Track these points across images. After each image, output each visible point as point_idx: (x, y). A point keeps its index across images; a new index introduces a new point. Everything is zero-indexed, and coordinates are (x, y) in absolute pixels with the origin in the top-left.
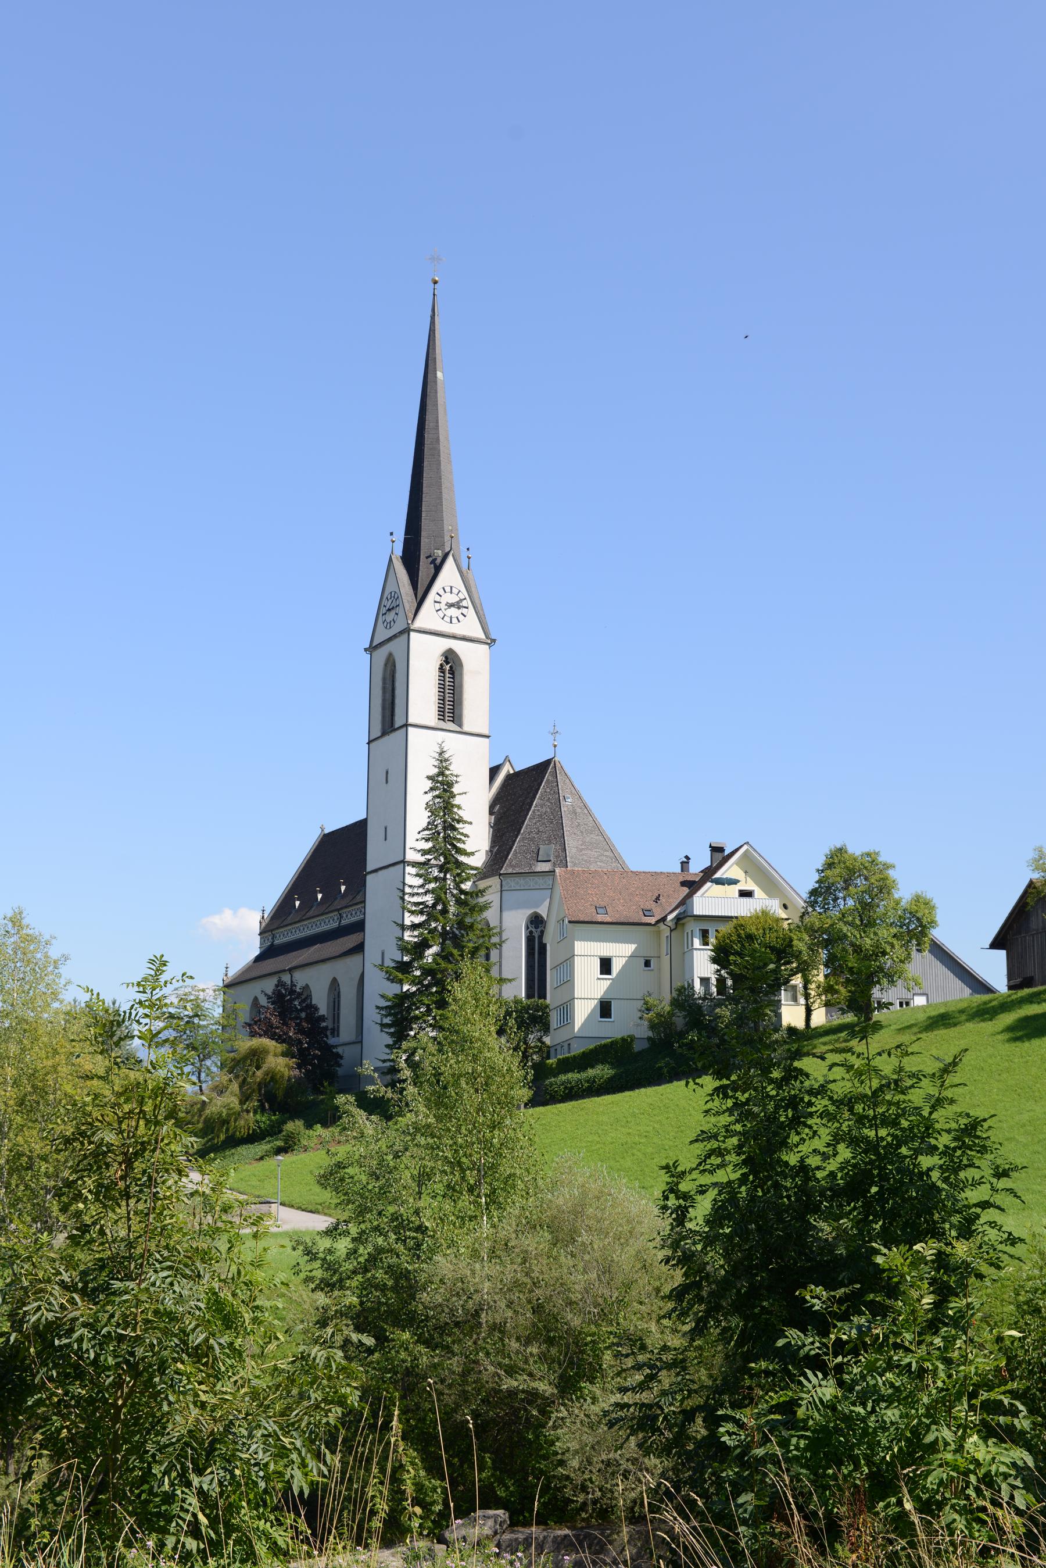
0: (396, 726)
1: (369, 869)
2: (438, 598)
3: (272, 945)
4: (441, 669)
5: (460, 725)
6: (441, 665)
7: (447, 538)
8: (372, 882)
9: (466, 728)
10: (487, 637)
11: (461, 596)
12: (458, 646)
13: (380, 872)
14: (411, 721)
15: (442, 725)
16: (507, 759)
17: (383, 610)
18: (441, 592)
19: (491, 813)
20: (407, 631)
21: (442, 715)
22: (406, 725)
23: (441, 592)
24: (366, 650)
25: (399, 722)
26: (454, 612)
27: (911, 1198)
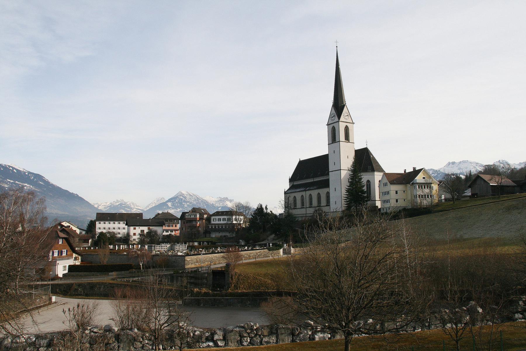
5: (349, 141)
9: (350, 142)
12: (348, 124)
13: (333, 172)
20: (339, 122)
25: (337, 140)
26: (347, 117)
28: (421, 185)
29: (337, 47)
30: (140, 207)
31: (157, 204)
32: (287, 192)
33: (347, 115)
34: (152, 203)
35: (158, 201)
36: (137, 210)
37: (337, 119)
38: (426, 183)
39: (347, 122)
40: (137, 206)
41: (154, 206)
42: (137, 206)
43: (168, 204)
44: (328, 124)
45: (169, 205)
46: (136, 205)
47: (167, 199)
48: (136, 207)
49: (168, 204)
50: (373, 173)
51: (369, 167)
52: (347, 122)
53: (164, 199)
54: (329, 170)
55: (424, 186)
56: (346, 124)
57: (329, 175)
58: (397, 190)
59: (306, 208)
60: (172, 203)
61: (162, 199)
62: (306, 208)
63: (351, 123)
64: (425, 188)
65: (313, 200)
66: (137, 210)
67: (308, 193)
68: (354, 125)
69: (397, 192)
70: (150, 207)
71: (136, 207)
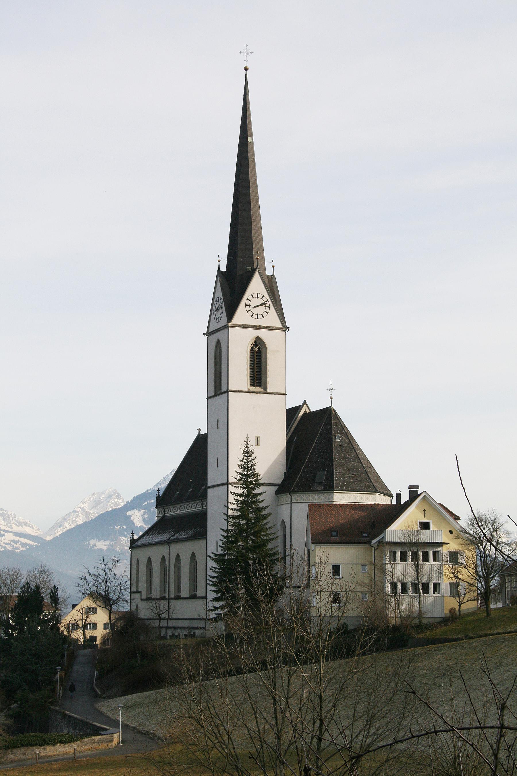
0: (223, 391)
1: (209, 485)
2: (248, 303)
3: (164, 516)
4: (252, 351)
5: (265, 389)
6: (252, 348)
7: (255, 261)
8: (210, 492)
9: (269, 390)
10: (283, 326)
11: (265, 299)
12: (263, 334)
13: (215, 489)
14: (230, 389)
15: (253, 389)
16: (305, 402)
17: (214, 309)
18: (250, 298)
19: (334, 410)
20: (227, 327)
21: (252, 384)
22: (228, 391)
23: (250, 298)
24: (204, 334)
25: (224, 389)
26: (260, 310)
27: (26, 626)
28: (394, 549)
29: (246, 69)
30: (32, 528)
31: (94, 514)
32: (139, 543)
33: (261, 302)
34: (75, 511)
35: (97, 503)
36: (17, 539)
37: (224, 321)
38: (410, 544)
39: (260, 327)
40: (20, 524)
41: (80, 522)
42: (20, 524)
43: (130, 516)
44: (210, 331)
45: (135, 521)
46: (17, 521)
47: (128, 498)
48: (14, 526)
49: (130, 516)
50: (328, 496)
51: (321, 475)
52: (260, 327)
53: (119, 496)
54: (206, 480)
55: (401, 552)
56: (252, 335)
57: (204, 496)
58: (336, 562)
59: (169, 599)
60: (144, 513)
61: (110, 497)
62: (169, 599)
63: (277, 329)
64: (426, 559)
65: (154, 584)
66: (17, 539)
67: (175, 549)
68: (288, 333)
69: (336, 569)
70: (68, 526)
71: (14, 526)
